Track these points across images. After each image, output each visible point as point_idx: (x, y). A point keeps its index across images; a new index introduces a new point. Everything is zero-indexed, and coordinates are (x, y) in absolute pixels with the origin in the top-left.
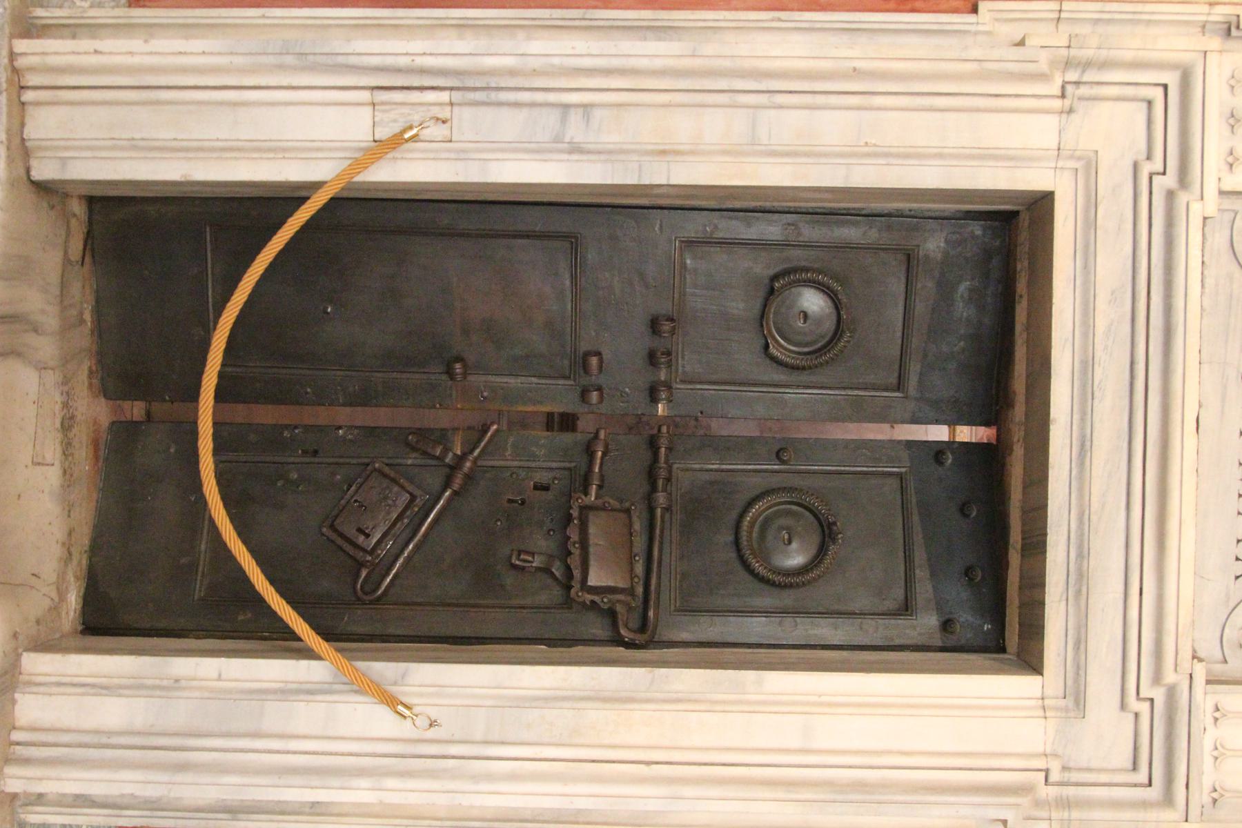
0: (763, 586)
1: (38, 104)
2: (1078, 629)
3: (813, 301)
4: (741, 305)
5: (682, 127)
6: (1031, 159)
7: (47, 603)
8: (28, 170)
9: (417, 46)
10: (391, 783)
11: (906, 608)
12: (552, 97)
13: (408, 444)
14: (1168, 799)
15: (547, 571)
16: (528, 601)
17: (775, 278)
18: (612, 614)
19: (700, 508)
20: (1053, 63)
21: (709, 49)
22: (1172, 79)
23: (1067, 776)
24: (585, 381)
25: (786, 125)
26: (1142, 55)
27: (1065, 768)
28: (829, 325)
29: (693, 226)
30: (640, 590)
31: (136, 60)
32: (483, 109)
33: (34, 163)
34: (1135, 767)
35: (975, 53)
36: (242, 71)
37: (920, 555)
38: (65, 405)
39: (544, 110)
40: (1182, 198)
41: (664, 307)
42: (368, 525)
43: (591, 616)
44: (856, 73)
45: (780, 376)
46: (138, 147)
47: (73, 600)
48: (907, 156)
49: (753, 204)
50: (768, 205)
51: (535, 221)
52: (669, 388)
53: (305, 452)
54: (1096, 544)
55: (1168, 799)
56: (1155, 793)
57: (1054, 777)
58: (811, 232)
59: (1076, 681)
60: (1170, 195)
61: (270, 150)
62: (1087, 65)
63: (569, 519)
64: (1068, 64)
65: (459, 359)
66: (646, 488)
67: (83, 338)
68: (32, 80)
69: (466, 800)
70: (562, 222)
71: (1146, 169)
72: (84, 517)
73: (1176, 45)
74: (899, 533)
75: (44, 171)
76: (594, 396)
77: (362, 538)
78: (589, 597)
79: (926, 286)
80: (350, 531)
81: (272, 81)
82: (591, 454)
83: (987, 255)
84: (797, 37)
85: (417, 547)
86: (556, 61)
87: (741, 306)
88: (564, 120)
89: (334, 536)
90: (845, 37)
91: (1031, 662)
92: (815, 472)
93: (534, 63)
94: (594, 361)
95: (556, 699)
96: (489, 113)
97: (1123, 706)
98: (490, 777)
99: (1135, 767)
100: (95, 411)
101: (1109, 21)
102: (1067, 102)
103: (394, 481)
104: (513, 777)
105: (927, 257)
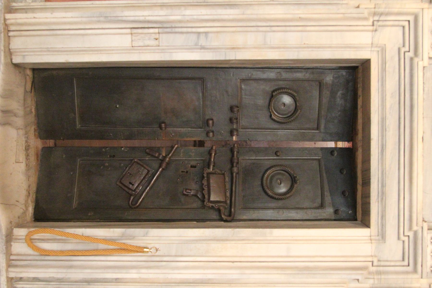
1: (15, 36)
3: (287, 99)
4: (262, 102)
5: (240, 39)
6: (362, 48)
7: (21, 211)
8: (11, 60)
9: (146, 13)
10: (143, 271)
11: (322, 206)
12: (194, 30)
13: (146, 153)
14: (415, 271)
15: (196, 196)
17: (274, 91)
18: (219, 211)
19: (249, 172)
20: (369, 14)
21: (249, 12)
22: (411, 18)
24: (208, 129)
25: (276, 38)
27: (379, 261)
28: (292, 108)
29: (244, 74)
30: (228, 202)
31: (48, 20)
33: (14, 57)
34: (403, 260)
35: (342, 11)
36: (85, 23)
38: (26, 142)
40: (416, 60)
41: (235, 103)
42: (133, 181)
43: (212, 211)
44: (301, 19)
45: (276, 126)
46: (49, 51)
47: (31, 210)
48: (319, 48)
52: (237, 130)
55: (415, 271)
56: (410, 268)
57: (375, 264)
58: (285, 75)
60: (411, 59)
62: (381, 14)
63: (203, 177)
64: (375, 14)
65: (164, 122)
66: (229, 166)
67: (32, 118)
69: (170, 276)
71: (403, 50)
72: (34, 180)
75: (17, 60)
76: (211, 134)
78: (211, 205)
80: (127, 184)
82: (210, 154)
83: (348, 82)
84: (279, 7)
87: (262, 101)
88: (198, 38)
89: (121, 185)
91: (366, 224)
93: (187, 18)
94: (211, 122)
95: (200, 240)
96: (172, 35)
97: (399, 238)
98: (178, 268)
99: (403, 260)
100: (37, 144)
102: (375, 28)
103: (143, 166)
105: (326, 83)
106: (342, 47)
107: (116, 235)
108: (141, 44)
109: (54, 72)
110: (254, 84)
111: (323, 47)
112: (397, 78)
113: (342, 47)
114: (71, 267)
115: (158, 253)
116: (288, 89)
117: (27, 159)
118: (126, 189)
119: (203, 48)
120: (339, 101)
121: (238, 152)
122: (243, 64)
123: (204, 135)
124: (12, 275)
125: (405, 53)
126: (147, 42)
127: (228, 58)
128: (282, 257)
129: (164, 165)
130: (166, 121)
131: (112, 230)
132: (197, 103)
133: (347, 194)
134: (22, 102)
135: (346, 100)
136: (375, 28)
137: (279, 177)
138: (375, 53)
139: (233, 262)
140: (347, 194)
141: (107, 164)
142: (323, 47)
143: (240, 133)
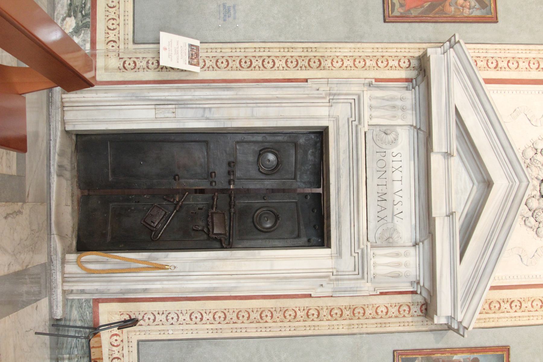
0: (259, 232)
1: (68, 111)
2: (339, 236)
3: (271, 157)
4: (252, 158)
5: (234, 112)
6: (322, 118)
7: (70, 242)
8: (65, 128)
9: (166, 94)
10: (165, 282)
11: (299, 236)
12: (201, 106)
14: (363, 278)
16: (198, 239)
17: (261, 151)
18: (220, 241)
19: (244, 212)
20: (326, 94)
21: (240, 93)
22: (356, 97)
23: (338, 273)
24: (211, 180)
25: (260, 111)
26: (348, 92)
27: (337, 271)
28: (275, 163)
29: (239, 138)
30: (228, 234)
31: (94, 99)
32: (183, 109)
33: (66, 126)
34: (355, 270)
35: (307, 92)
36: (121, 101)
37: (302, 222)
38: (72, 190)
39: (199, 109)
40: (359, 127)
41: (232, 159)
42: (154, 220)
44: (278, 98)
45: (263, 177)
47: (74, 243)
48: (292, 118)
49: (254, 132)
50: (258, 131)
51: (196, 137)
52: (234, 181)
53: (136, 202)
54: (342, 214)
55: (363, 278)
56: (360, 276)
57: (335, 273)
58: (269, 138)
59: (339, 249)
60: (357, 126)
61: (129, 121)
62: (335, 95)
63: (208, 216)
64: (330, 94)
65: (178, 175)
66: (228, 208)
67: (75, 173)
68: (66, 105)
69: (185, 286)
70: (204, 138)
71: (351, 120)
72: (76, 220)
73: (355, 89)
74: (296, 217)
75: (69, 128)
76: (214, 183)
77: (152, 224)
78: (214, 236)
79: (300, 151)
80: (149, 222)
81: (129, 103)
82: (213, 199)
83: (316, 143)
84: (262, 89)
85: (167, 226)
86: (202, 97)
87: (251, 158)
88: (204, 111)
89: (144, 224)
90: (275, 89)
91: (329, 246)
92: (273, 202)
93: (196, 97)
94: (213, 174)
95: (207, 260)
96: (185, 110)
97: (351, 255)
99: (355, 270)
100: (77, 192)
101: (340, 83)
102: (330, 104)
103: (160, 208)
104: (197, 280)
105: (300, 144)
106: (308, 118)
107: (144, 257)
108: (162, 116)
109: (93, 137)
110: (246, 145)
111: (294, 118)
112: (347, 140)
113: (308, 118)
114: (111, 281)
115: (175, 270)
116: (272, 149)
117: (72, 204)
118: (148, 226)
119: (207, 119)
120: (310, 157)
121: (234, 197)
122: (237, 130)
123: (209, 184)
124: (66, 288)
125: (352, 121)
126: (167, 115)
127: (226, 126)
128: (267, 270)
129: (178, 208)
130: (179, 174)
131: (141, 254)
132: (203, 160)
133: (317, 227)
134: (70, 159)
135: (315, 157)
136: (330, 104)
137: (267, 215)
138: (332, 122)
139: (231, 275)
140: (317, 227)
141: (133, 208)
142: (294, 118)
143: (236, 183)
